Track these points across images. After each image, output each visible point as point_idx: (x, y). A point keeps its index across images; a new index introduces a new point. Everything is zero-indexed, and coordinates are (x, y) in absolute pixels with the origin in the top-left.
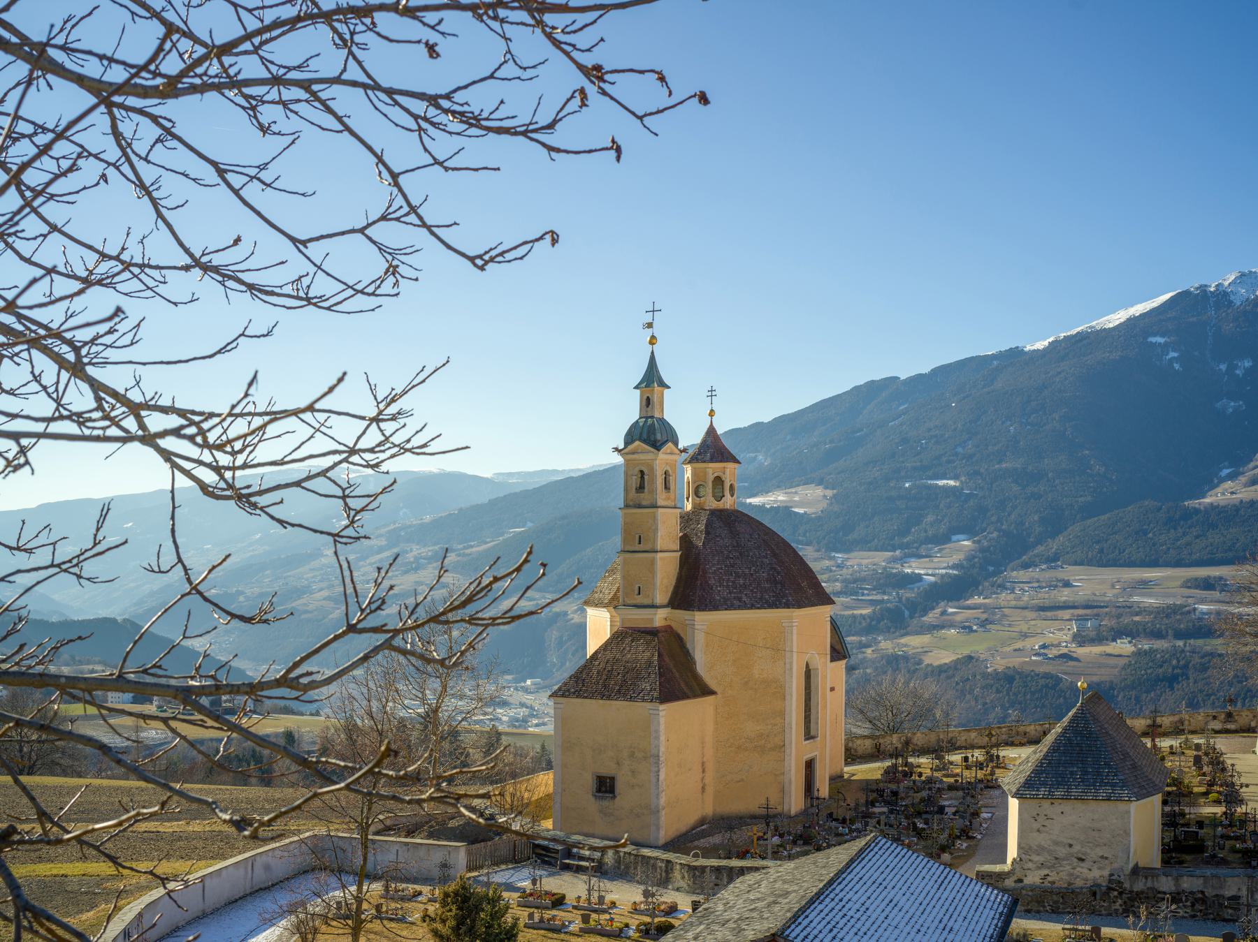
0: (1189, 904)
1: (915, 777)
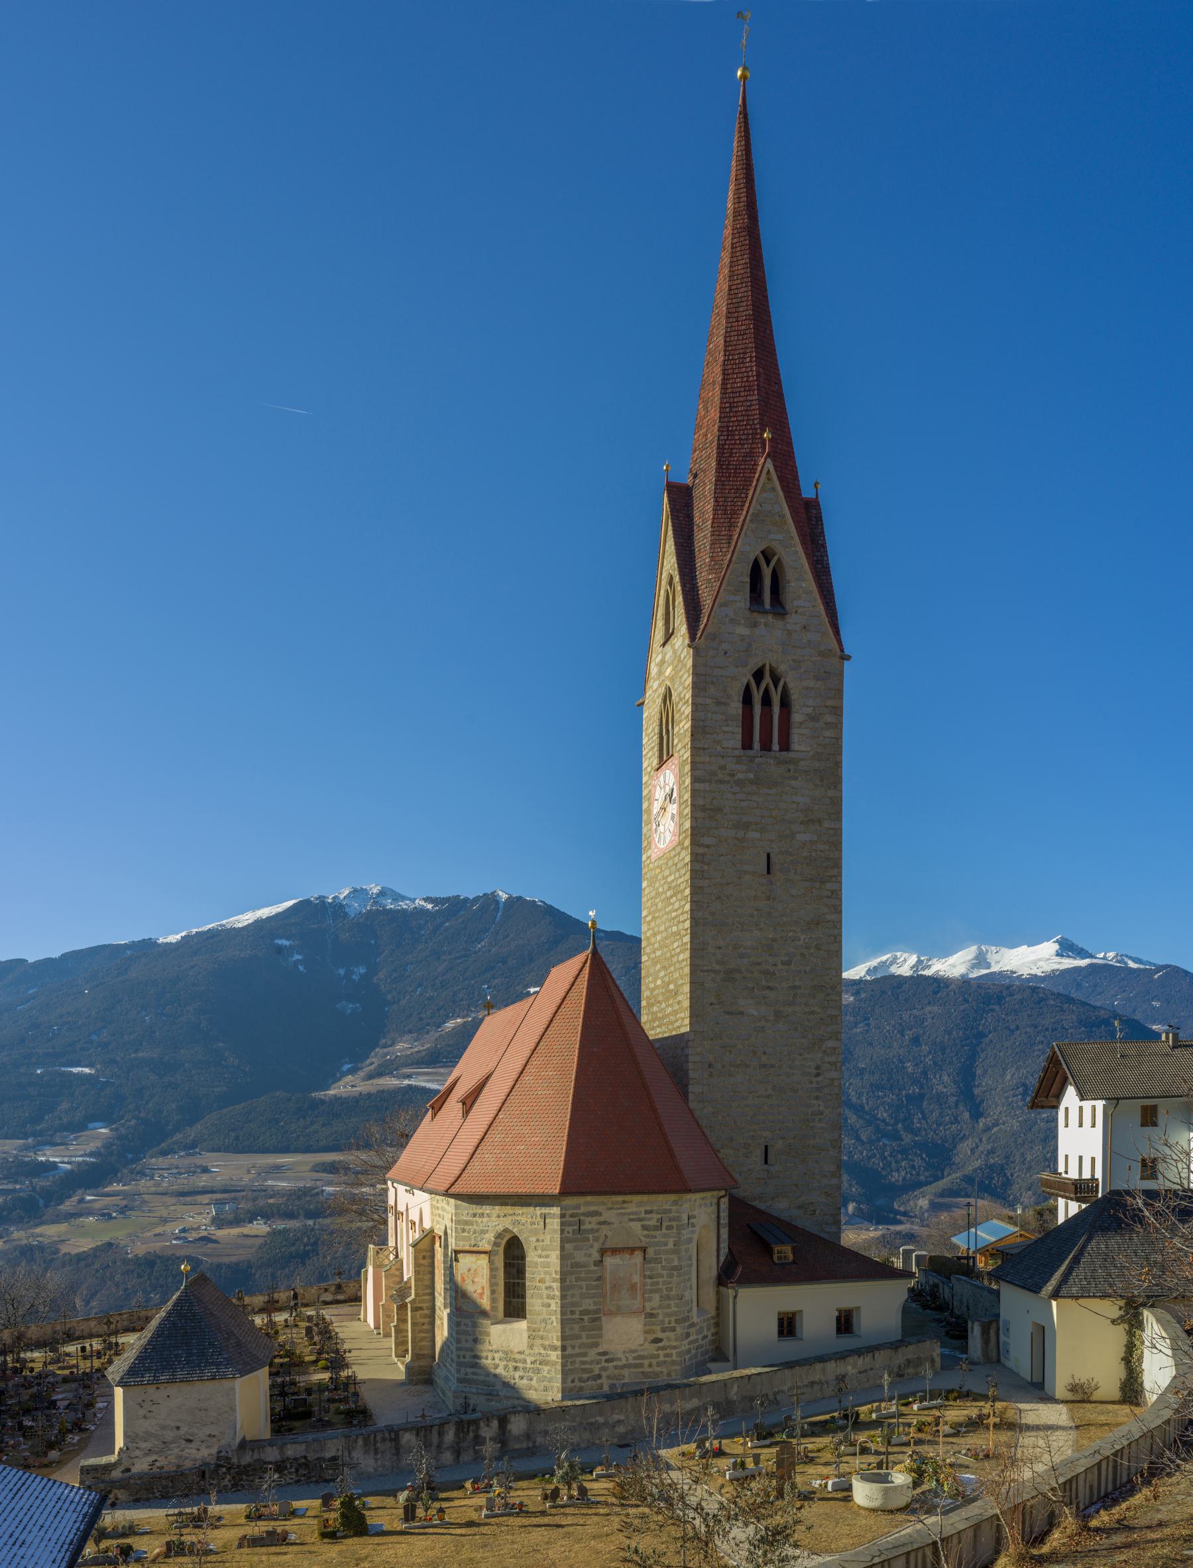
0: (293, 1470)
1: (26, 1373)
